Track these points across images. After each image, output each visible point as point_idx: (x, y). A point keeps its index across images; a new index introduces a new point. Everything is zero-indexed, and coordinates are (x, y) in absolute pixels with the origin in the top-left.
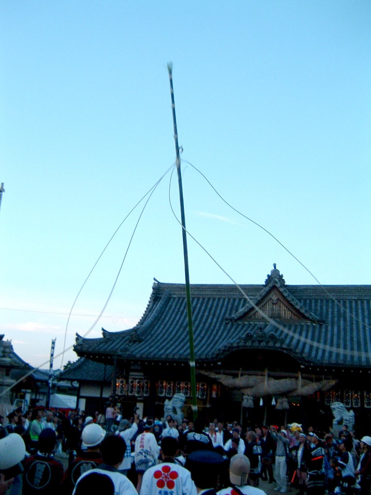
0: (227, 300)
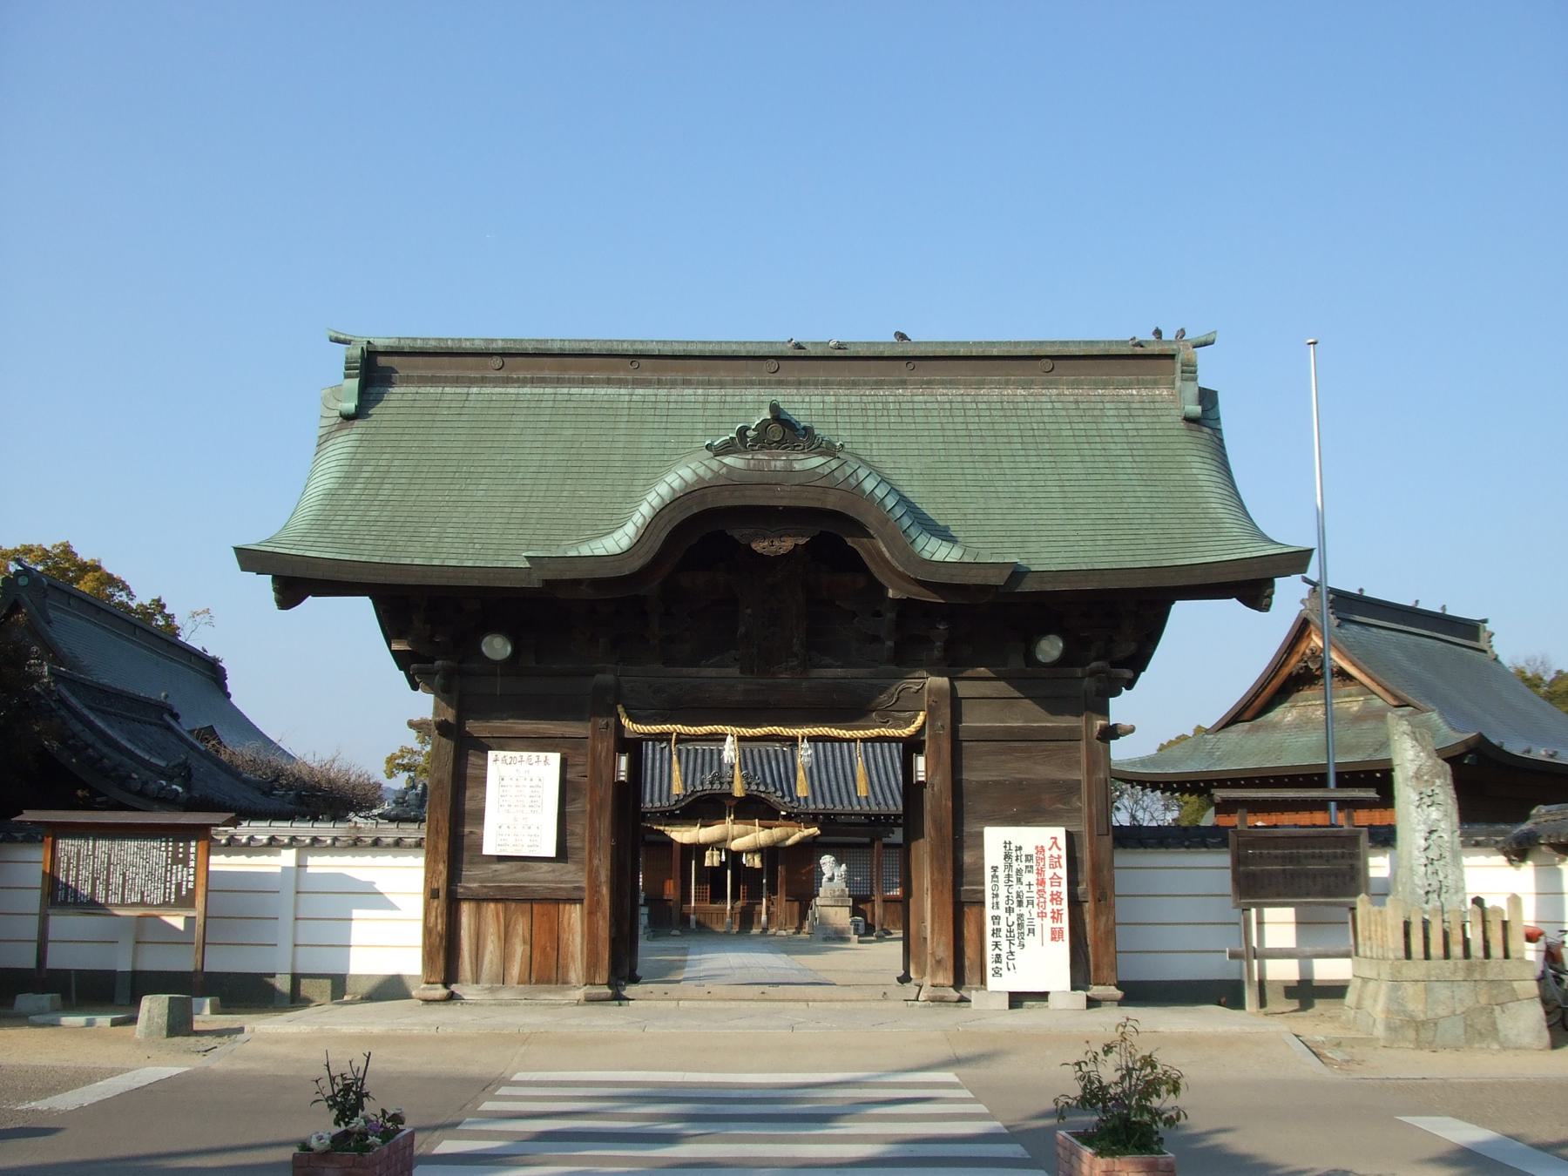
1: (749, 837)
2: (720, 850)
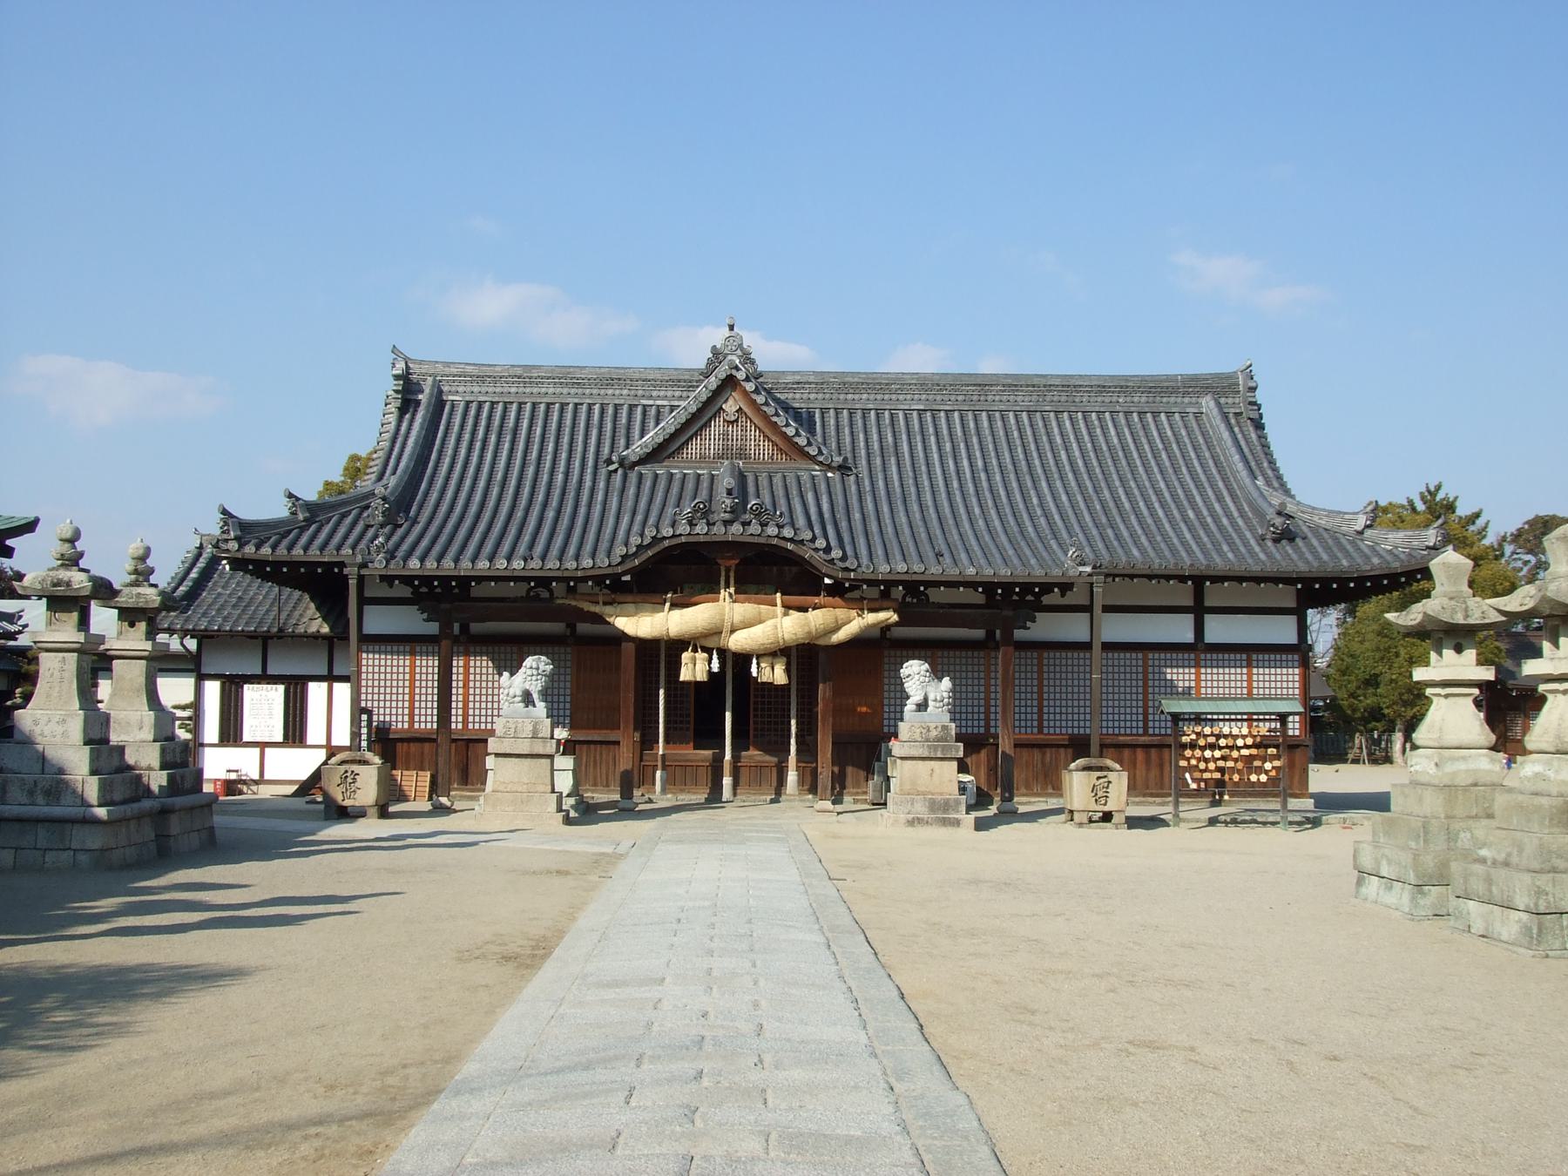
0: (597, 408)
1: (761, 626)
2: (708, 650)
